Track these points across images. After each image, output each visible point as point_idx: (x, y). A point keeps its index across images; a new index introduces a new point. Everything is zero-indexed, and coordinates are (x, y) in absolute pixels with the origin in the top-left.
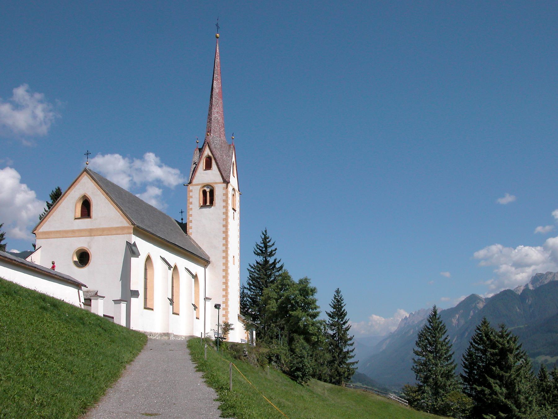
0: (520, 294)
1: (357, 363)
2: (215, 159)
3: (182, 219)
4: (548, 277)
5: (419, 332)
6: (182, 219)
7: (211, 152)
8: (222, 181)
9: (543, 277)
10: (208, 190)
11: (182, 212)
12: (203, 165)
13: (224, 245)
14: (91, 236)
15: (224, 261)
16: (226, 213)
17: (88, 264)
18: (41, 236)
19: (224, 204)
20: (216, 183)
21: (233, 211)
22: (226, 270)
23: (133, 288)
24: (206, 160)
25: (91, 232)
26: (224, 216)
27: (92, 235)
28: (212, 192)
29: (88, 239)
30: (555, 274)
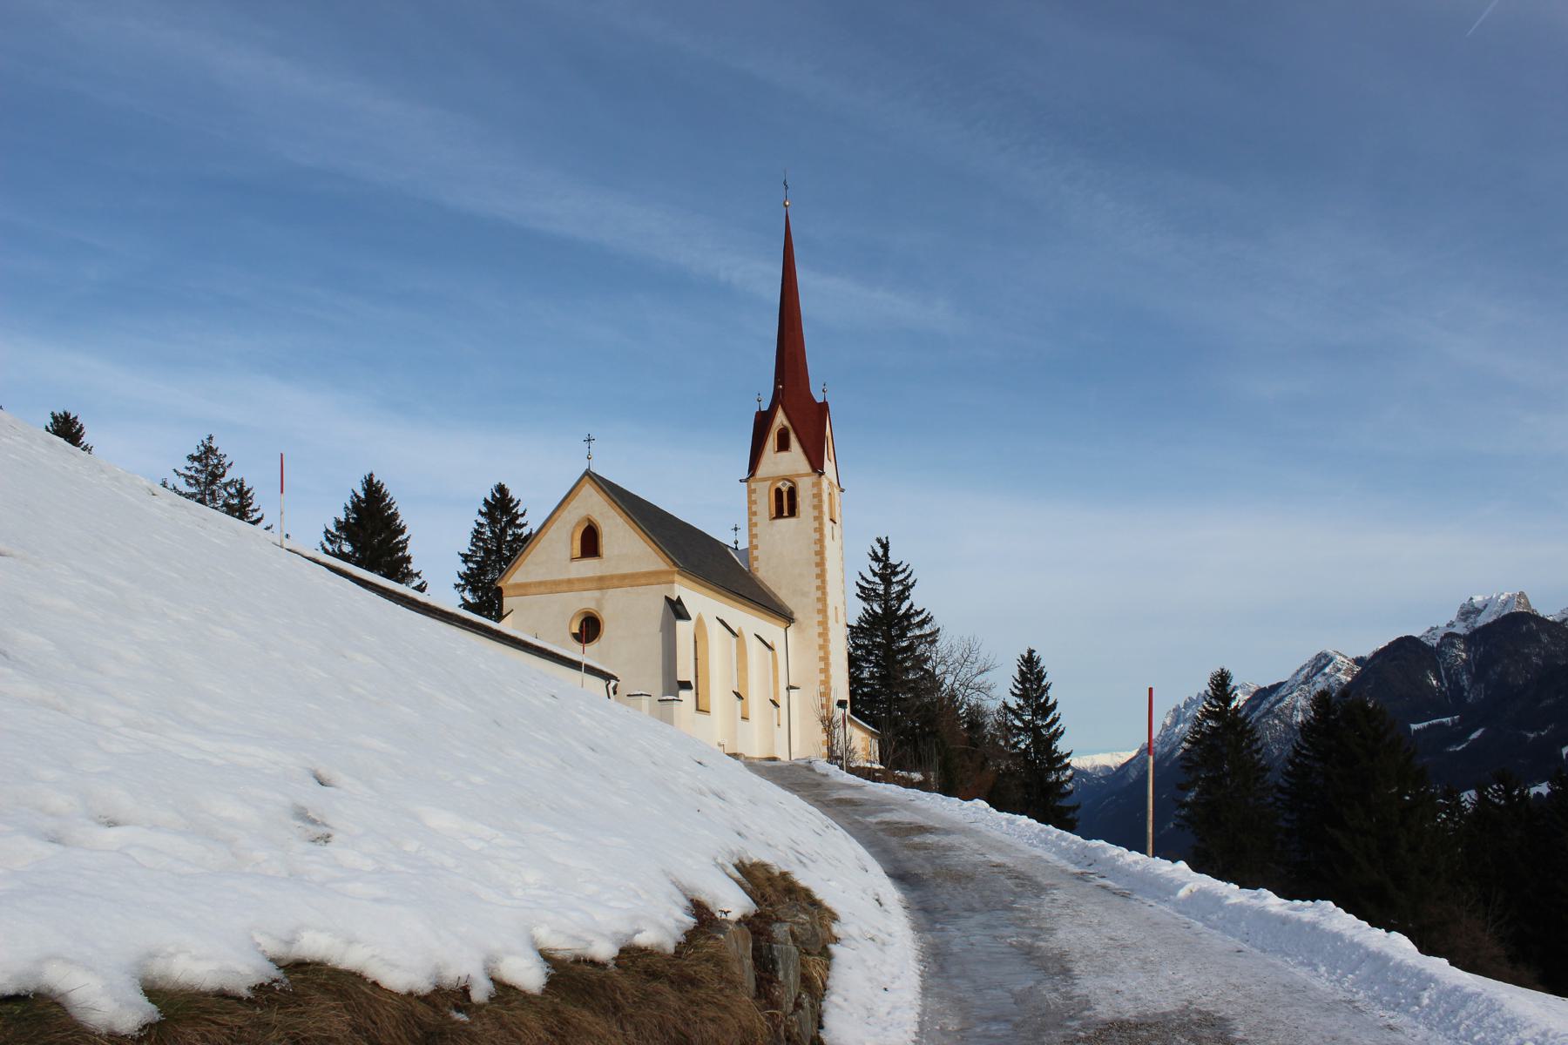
0: (1435, 645)
1: (1078, 807)
3: (736, 543)
5: (203, 445)
6: (736, 543)
10: (785, 489)
11: (736, 529)
13: (818, 588)
15: (820, 618)
16: (820, 530)
18: (512, 592)
19: (816, 513)
20: (799, 476)
21: (831, 523)
22: (824, 635)
23: (681, 677)
25: (602, 583)
26: (817, 536)
28: (792, 492)
29: (597, 594)
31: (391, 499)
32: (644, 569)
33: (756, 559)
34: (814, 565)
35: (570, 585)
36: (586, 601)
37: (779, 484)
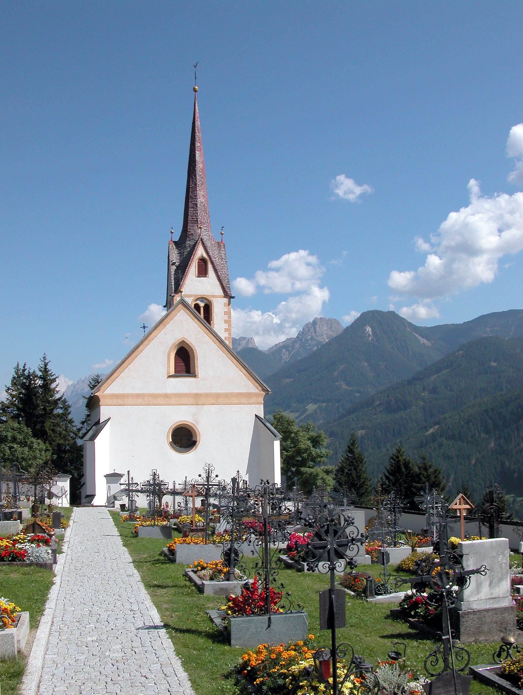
2: (212, 263)
4: (241, 343)
7: (207, 253)
8: (223, 295)
9: (235, 343)
10: (202, 305)
11: (144, 327)
12: (196, 268)
17: (195, 447)
18: (108, 401)
20: (215, 296)
24: (198, 263)
27: (200, 402)
29: (193, 409)
30: (249, 340)
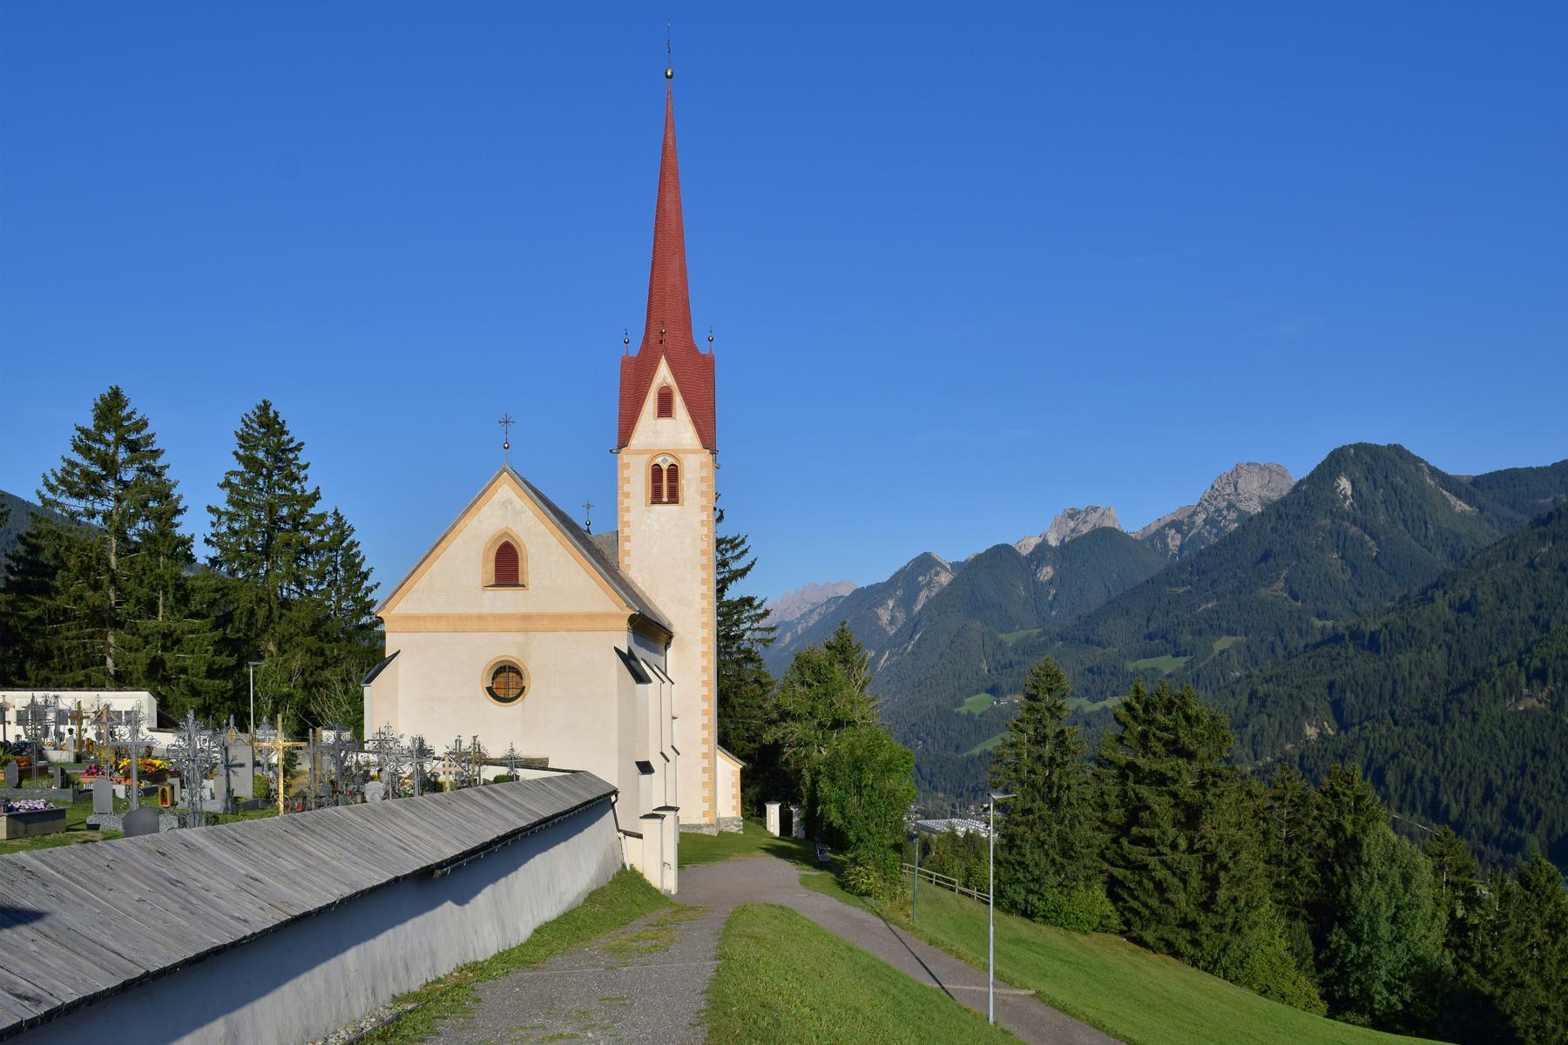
10: (665, 467)
11: (588, 506)
14: (526, 631)
20: (685, 451)
25: (528, 622)
28: (674, 471)
29: (520, 637)
31: (55, 474)
32: (563, 607)
33: (628, 553)
34: (699, 567)
35: (482, 622)
36: (506, 647)
37: (659, 460)
